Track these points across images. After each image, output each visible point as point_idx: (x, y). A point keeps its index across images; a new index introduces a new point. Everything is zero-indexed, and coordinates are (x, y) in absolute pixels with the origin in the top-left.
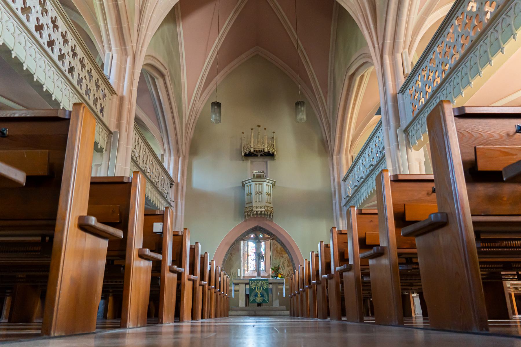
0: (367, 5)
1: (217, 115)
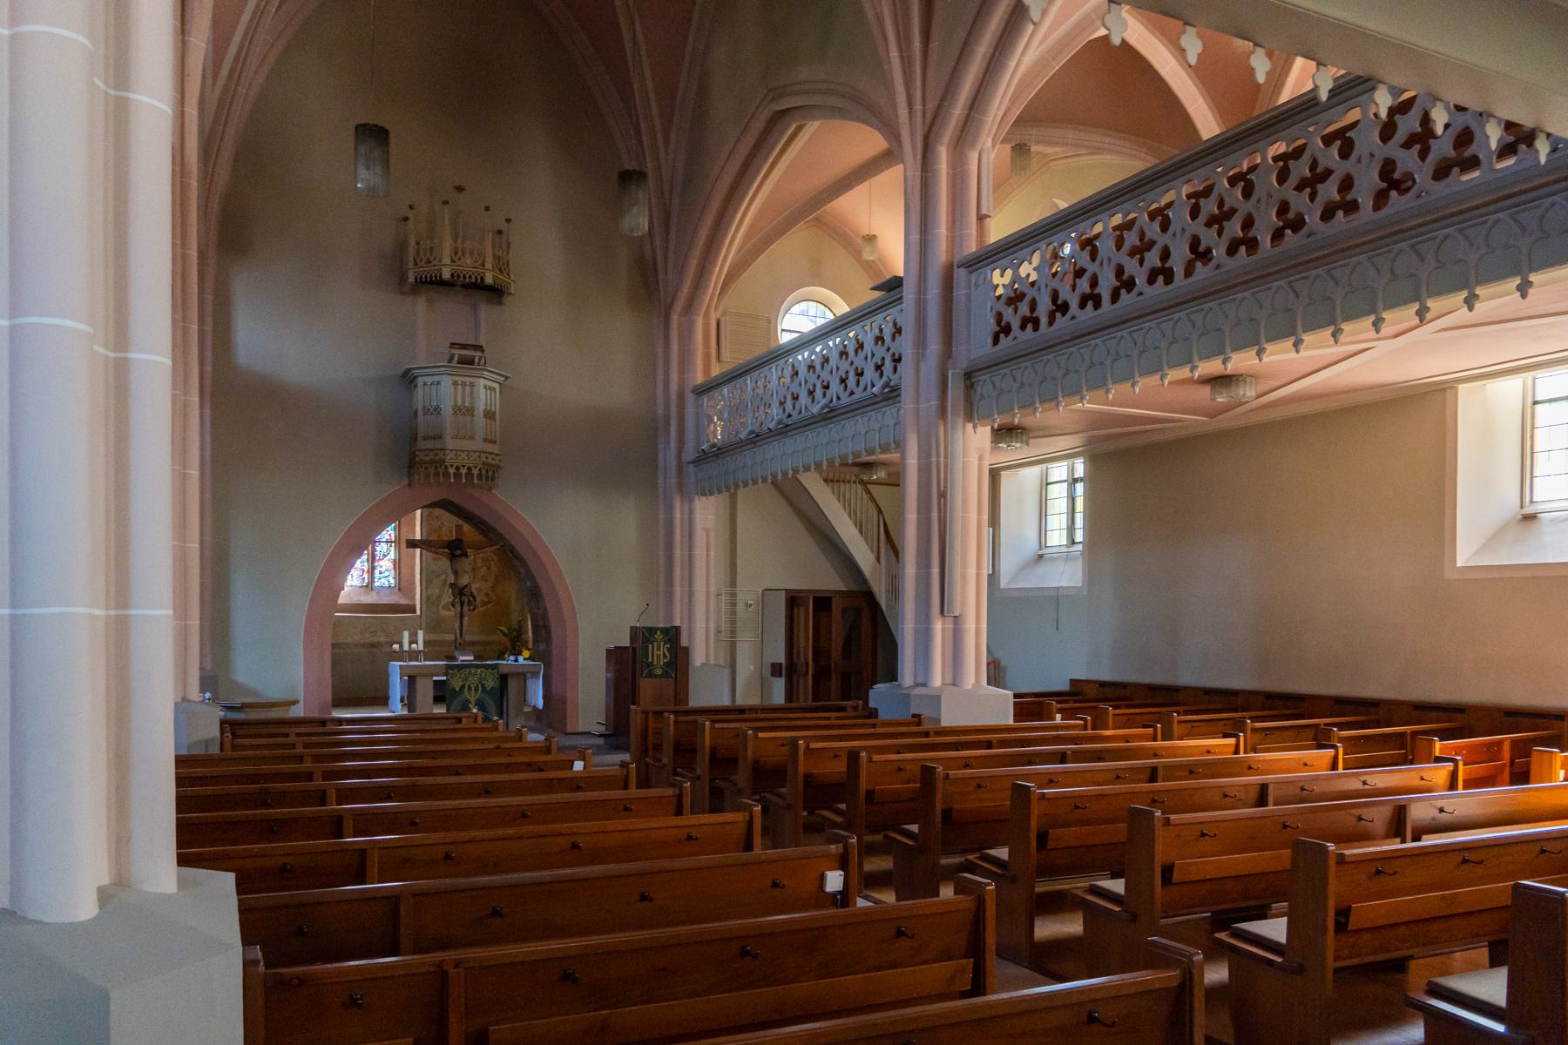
1: (378, 170)
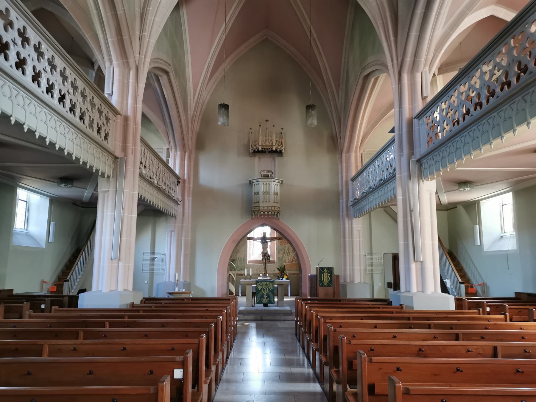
0: (388, 14)
1: (225, 118)
